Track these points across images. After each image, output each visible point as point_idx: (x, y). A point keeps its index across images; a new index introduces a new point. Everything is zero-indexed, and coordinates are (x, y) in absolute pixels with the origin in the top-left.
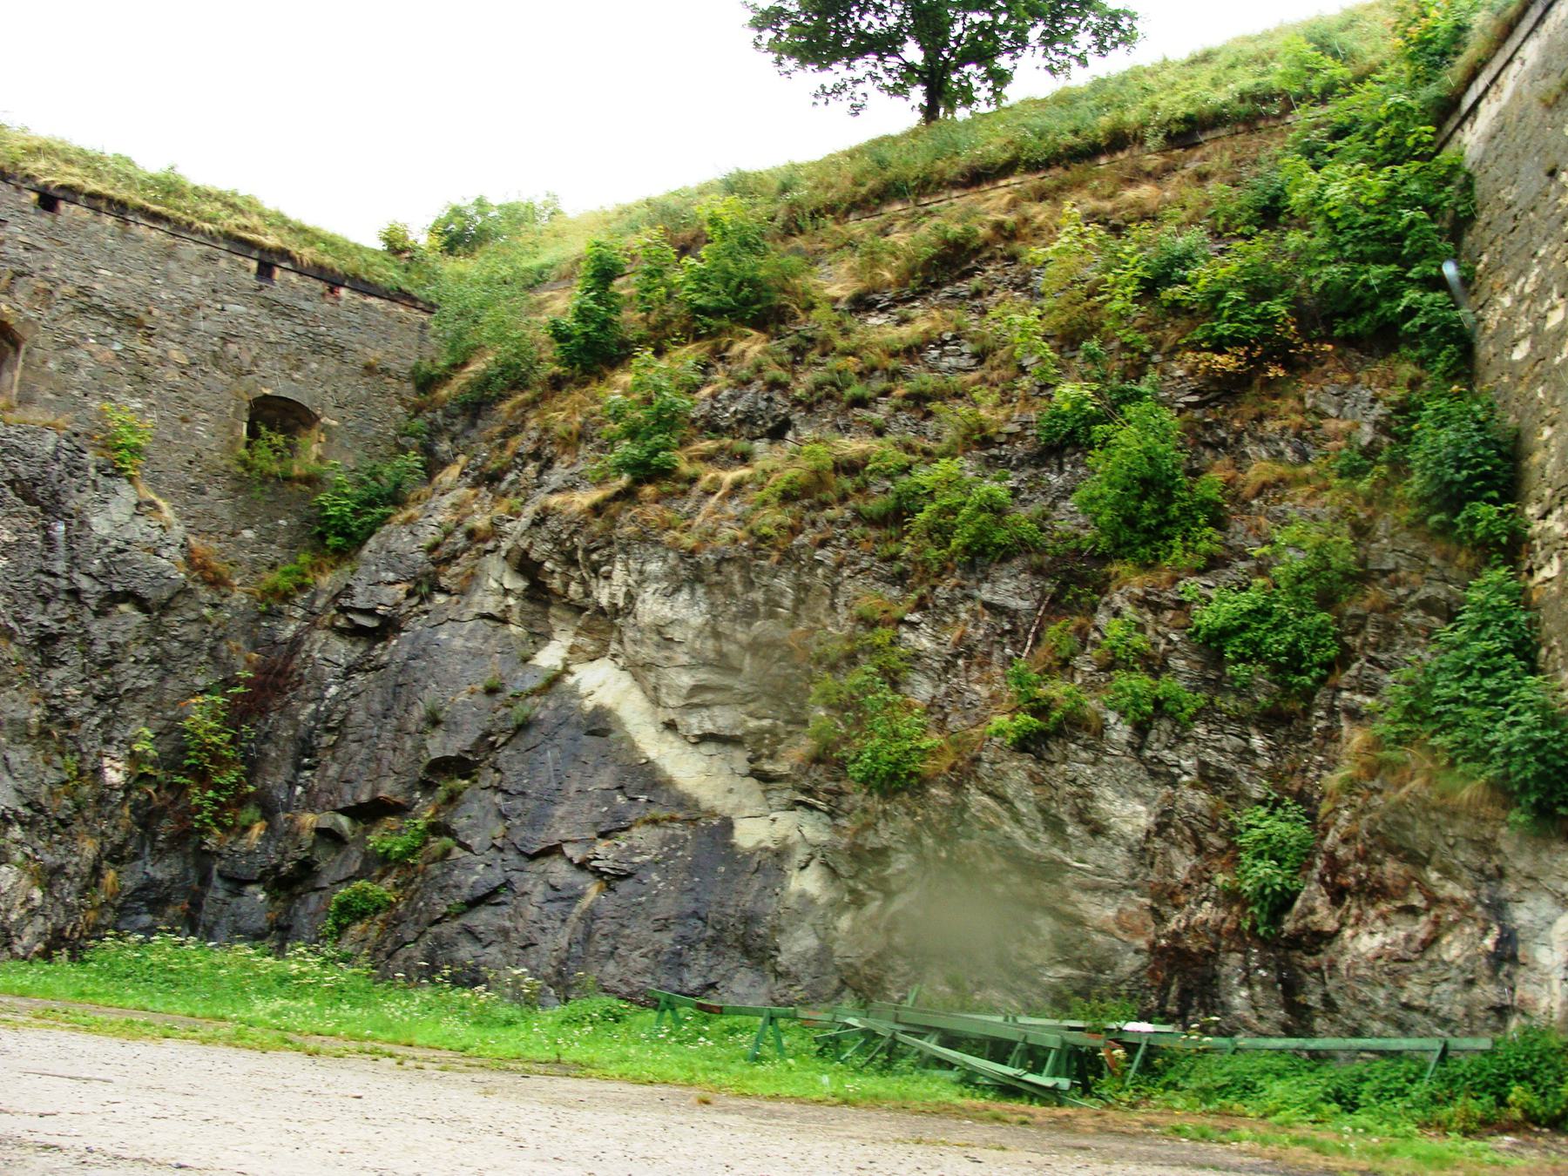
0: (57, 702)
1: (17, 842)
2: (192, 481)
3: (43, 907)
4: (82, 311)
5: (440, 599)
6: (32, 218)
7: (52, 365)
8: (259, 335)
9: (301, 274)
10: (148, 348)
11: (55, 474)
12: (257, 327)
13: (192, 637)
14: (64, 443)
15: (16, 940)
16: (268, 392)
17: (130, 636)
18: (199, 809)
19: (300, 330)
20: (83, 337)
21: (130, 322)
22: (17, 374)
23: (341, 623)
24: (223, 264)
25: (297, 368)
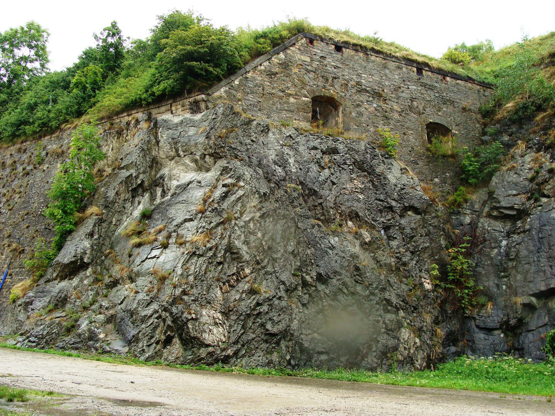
0: (398, 255)
1: (403, 318)
2: (412, 159)
3: (421, 346)
4: (359, 92)
5: (544, 200)
6: (334, 55)
7: (354, 114)
8: (423, 98)
9: (432, 72)
10: (386, 105)
11: (369, 158)
12: (422, 94)
13: (436, 224)
14: (368, 146)
15: (416, 362)
16: (431, 121)
17: (417, 224)
18: (463, 298)
19: (437, 95)
20: (362, 102)
21: (378, 95)
22: (340, 120)
23: (495, 213)
24: (404, 69)
25: (440, 111)
